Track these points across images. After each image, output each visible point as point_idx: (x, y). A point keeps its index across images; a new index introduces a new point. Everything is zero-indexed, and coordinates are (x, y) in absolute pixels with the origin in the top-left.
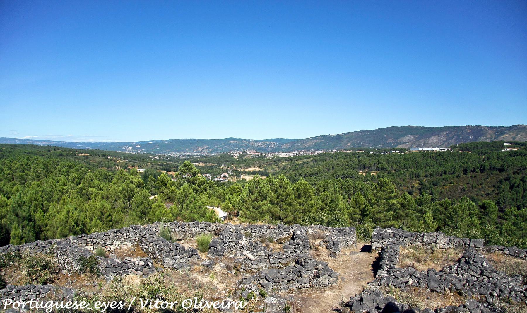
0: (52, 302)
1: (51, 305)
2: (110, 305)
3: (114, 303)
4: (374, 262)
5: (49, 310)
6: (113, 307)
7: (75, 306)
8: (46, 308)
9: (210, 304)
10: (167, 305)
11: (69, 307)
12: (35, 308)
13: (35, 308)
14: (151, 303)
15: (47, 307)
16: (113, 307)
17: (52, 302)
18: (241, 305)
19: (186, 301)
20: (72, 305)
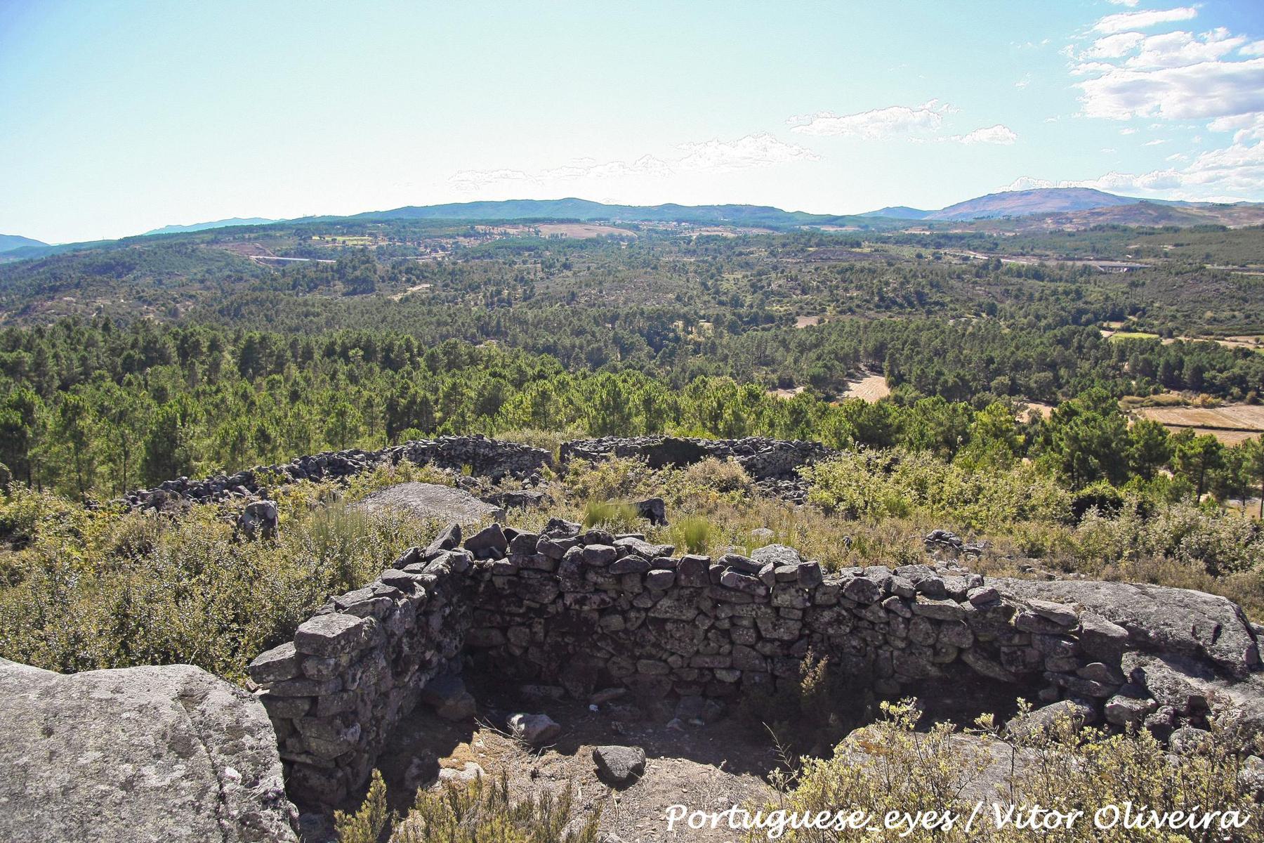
5: (774, 833)
6: (1176, 824)
7: (838, 821)
16: (1176, 824)
17: (783, 813)
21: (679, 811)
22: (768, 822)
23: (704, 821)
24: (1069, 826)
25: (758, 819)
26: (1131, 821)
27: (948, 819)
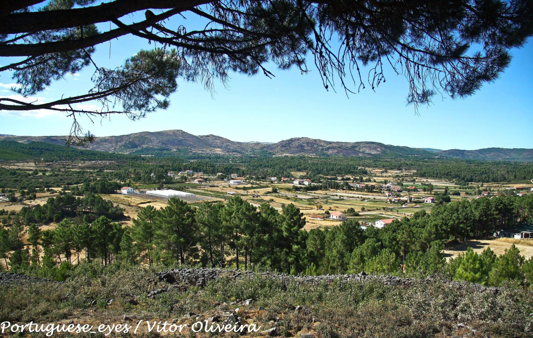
0: (53, 325)
2: (114, 328)
3: (228, 327)
4: (97, 30)
5: (49, 334)
6: (118, 330)
7: (77, 329)
10: (18, 329)
11: (86, 330)
12: (35, 331)
13: (35, 331)
15: (48, 330)
16: (101, 330)
17: (53, 325)
19: (196, 324)
20: (105, 328)
21: (7, 324)
22: (46, 329)
23: (18, 329)
24: (180, 331)
25: (63, 328)
26: (208, 328)
27: (126, 328)
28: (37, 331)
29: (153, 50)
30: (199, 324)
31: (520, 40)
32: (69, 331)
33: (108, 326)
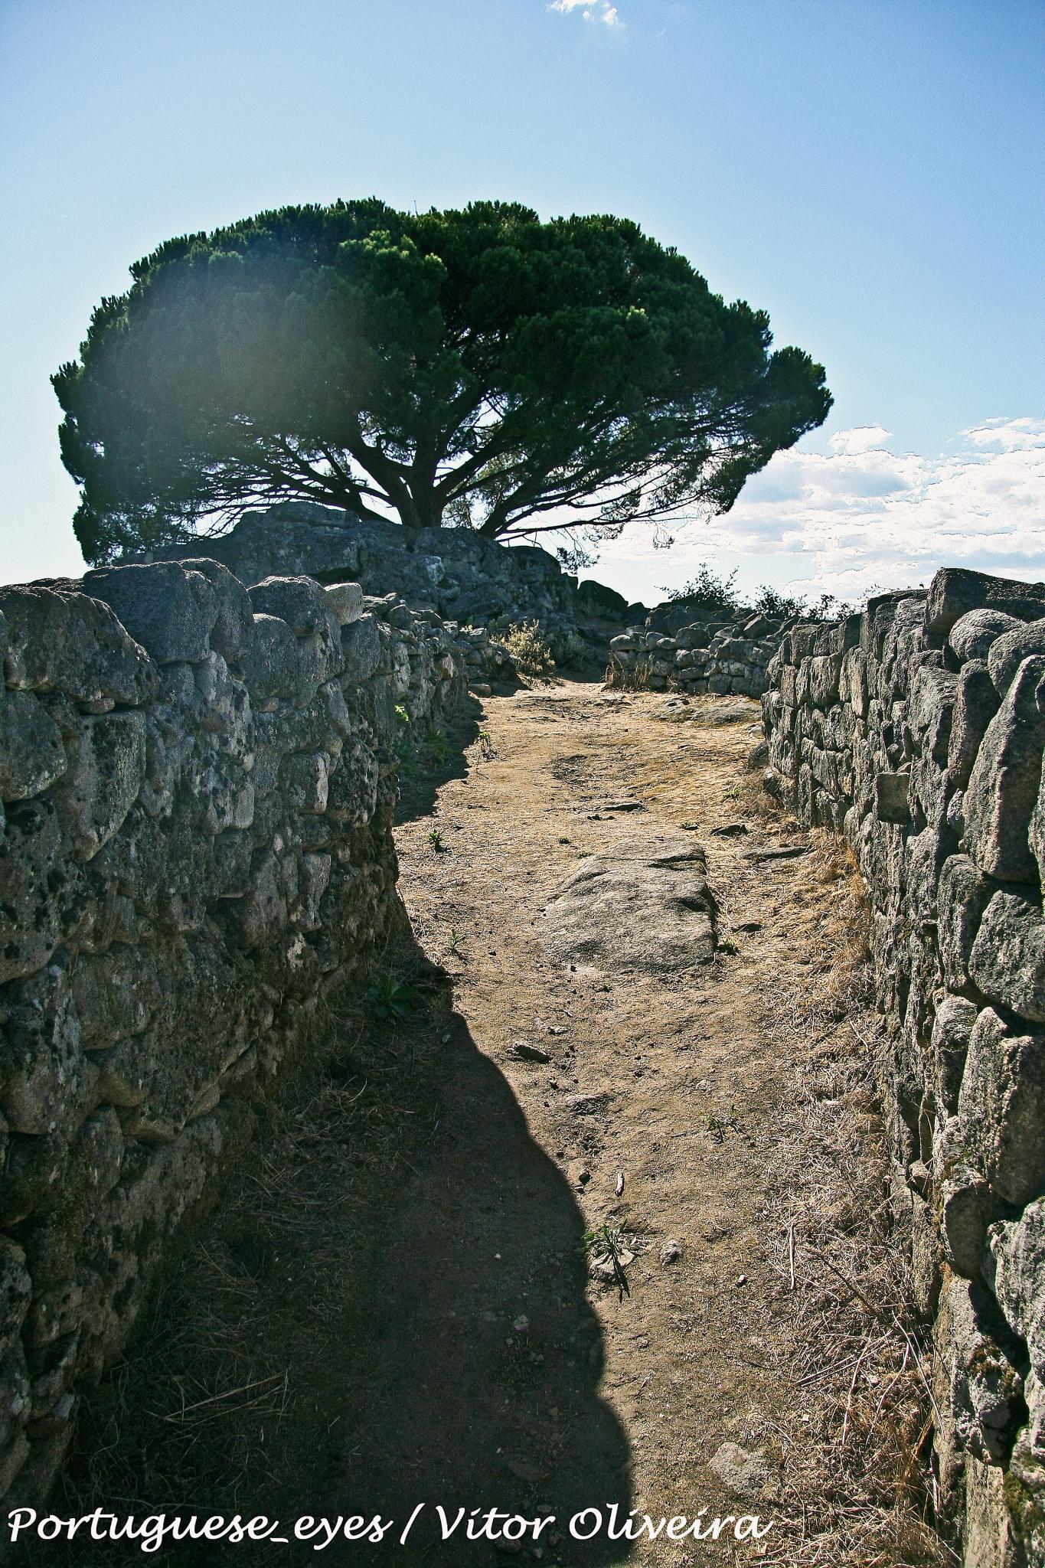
1: (154, 1532)
6: (303, 1533)
8: (141, 1538)
9: (655, 1526)
14: (471, 1522)
16: (353, 1533)
17: (161, 1519)
18: (754, 1527)
19: (582, 1515)
21: (25, 1517)
28: (113, 1536)
29: (490, 203)
30: (591, 1518)
31: (987, 1327)
32: (210, 1536)
33: (325, 1522)
